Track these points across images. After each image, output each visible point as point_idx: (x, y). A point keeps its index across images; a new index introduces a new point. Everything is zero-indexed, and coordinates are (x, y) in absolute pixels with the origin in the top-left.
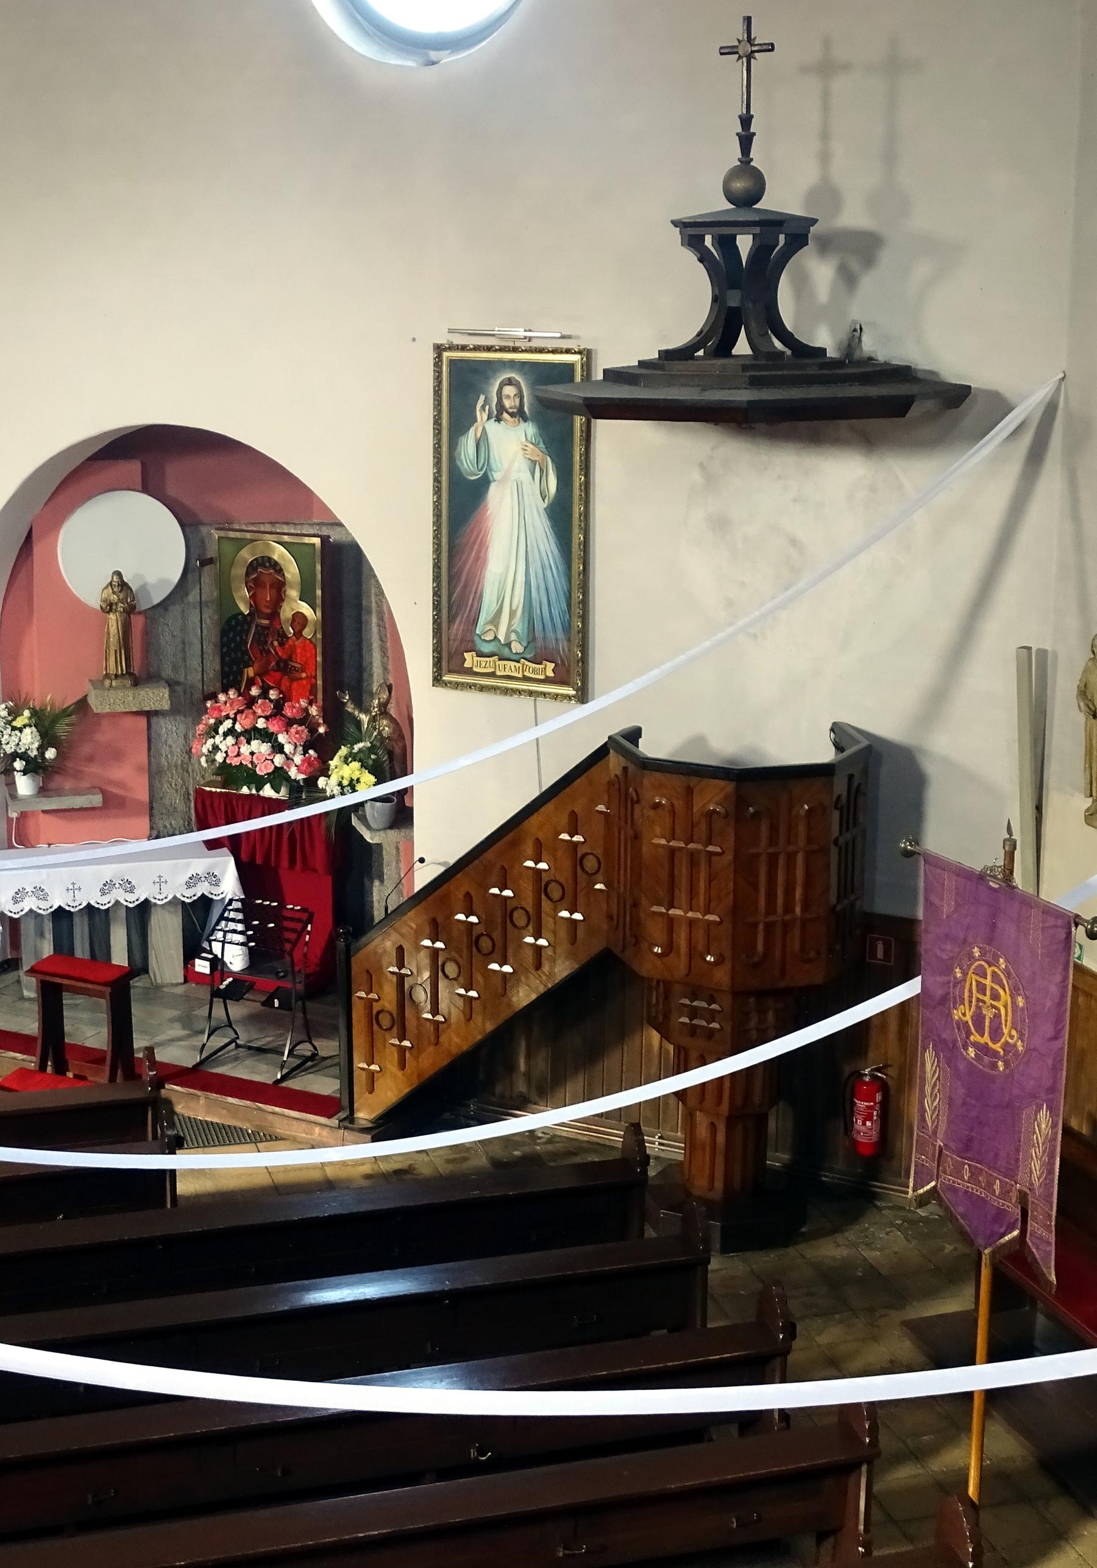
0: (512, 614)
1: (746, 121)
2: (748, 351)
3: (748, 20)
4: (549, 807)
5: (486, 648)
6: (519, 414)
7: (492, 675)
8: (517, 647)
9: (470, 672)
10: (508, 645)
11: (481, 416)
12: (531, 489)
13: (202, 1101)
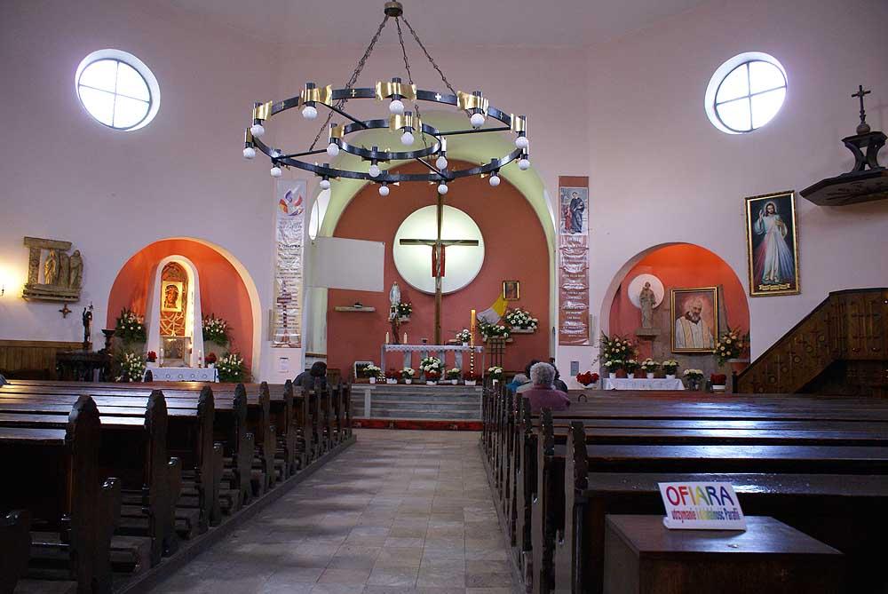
0: (775, 271)
1: (862, 112)
2: (869, 168)
3: (869, 92)
4: (807, 322)
5: (766, 283)
6: (774, 213)
7: (769, 290)
8: (777, 281)
9: (761, 291)
10: (774, 280)
11: (761, 216)
12: (779, 233)
13: (503, 555)
